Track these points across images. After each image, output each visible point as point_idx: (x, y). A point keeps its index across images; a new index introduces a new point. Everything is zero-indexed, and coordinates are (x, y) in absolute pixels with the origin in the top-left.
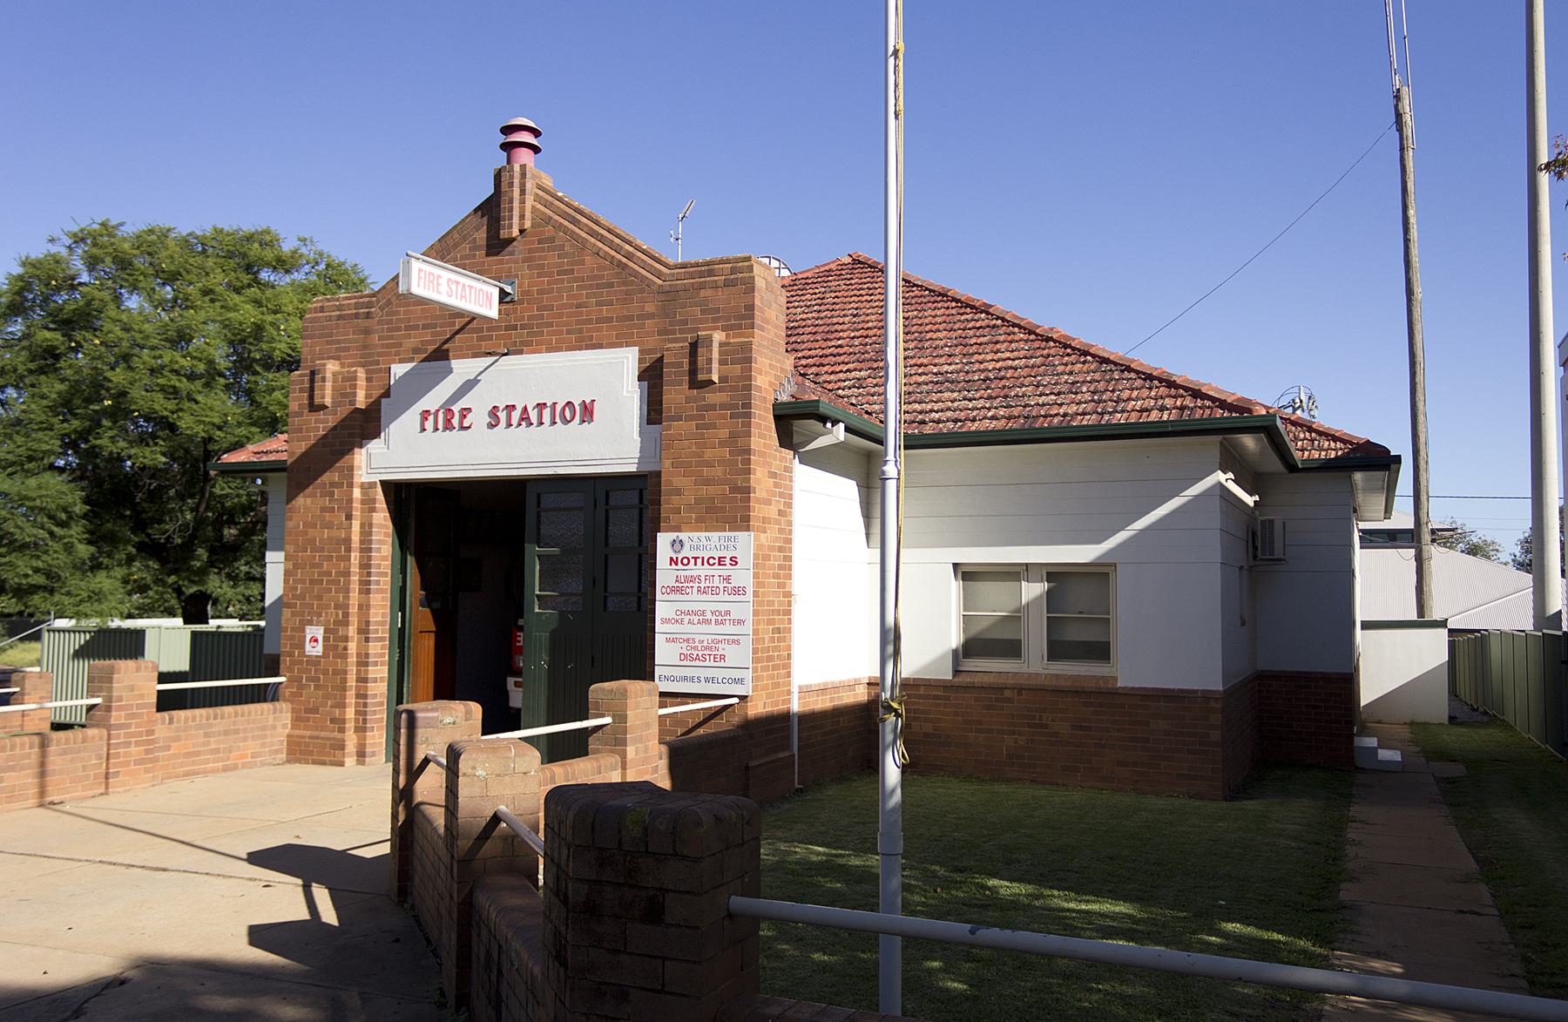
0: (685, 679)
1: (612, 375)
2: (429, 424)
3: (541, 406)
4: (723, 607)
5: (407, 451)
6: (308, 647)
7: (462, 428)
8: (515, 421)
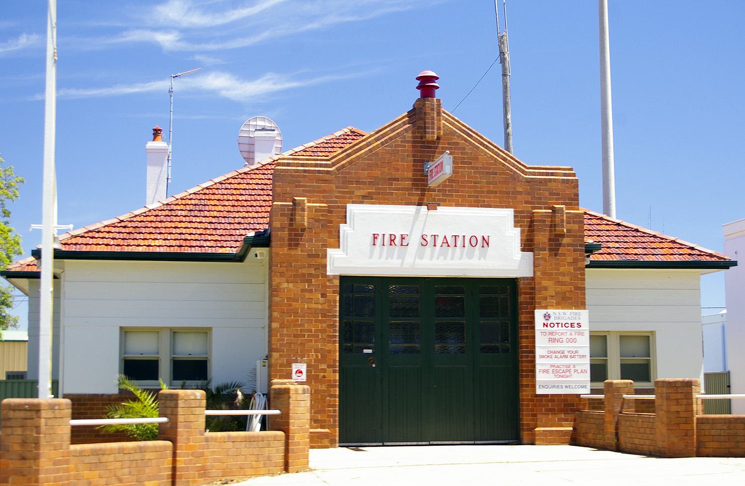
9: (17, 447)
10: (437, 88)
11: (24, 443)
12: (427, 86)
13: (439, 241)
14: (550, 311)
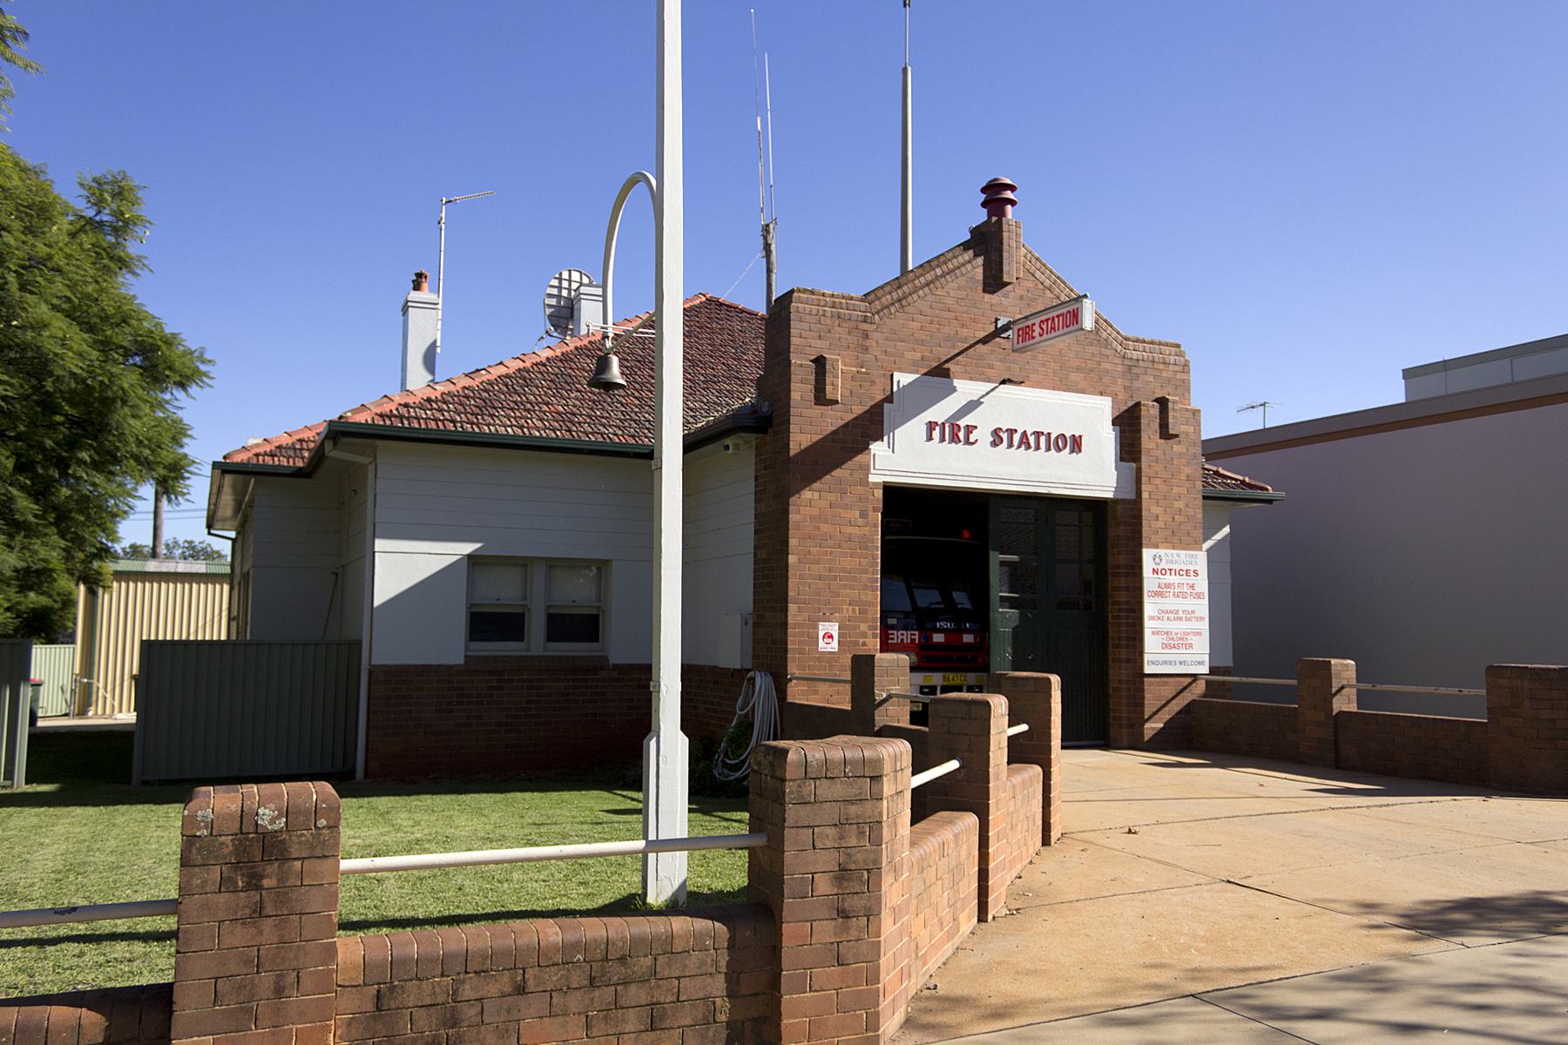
0: (1165, 663)
1: (1092, 416)
2: (936, 434)
3: (1038, 434)
4: (1190, 608)
5: (907, 457)
6: (821, 643)
7: (968, 442)
8: (1016, 442)
9: (824, 885)
10: (1013, 203)
11: (843, 874)
12: (995, 196)
13: (1016, 438)
14: (1161, 552)
